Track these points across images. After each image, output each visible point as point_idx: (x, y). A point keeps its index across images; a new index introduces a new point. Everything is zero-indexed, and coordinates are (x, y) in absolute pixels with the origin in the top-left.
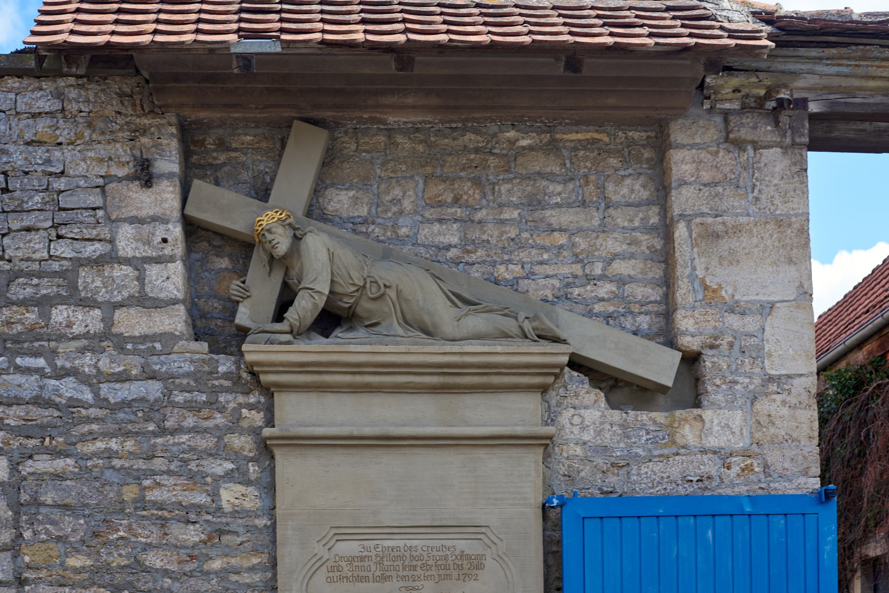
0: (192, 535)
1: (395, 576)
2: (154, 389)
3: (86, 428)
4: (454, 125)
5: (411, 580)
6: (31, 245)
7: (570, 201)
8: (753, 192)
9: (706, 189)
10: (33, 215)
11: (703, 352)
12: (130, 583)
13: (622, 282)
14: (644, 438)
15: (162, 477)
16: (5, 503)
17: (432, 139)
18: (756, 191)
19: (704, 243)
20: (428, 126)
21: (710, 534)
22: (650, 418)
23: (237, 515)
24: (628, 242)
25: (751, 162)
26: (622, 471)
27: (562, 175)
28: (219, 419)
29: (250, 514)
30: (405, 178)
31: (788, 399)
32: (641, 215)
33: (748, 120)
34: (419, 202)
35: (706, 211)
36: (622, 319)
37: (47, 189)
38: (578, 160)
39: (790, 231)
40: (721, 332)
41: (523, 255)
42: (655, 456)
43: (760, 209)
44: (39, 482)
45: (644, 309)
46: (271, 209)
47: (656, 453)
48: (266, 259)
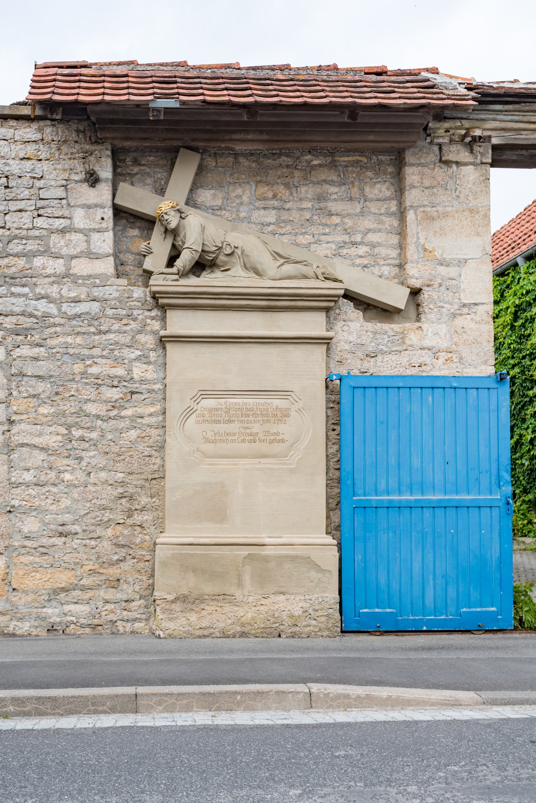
0: (114, 394)
1: (236, 420)
2: (95, 307)
3: (53, 330)
4: (274, 152)
5: (246, 422)
6: (22, 220)
7: (342, 197)
8: (455, 192)
9: (426, 191)
10: (24, 202)
11: (422, 288)
12: (77, 423)
13: (373, 246)
14: (386, 340)
15: (98, 359)
16: (2, 375)
17: (261, 160)
18: (457, 192)
19: (425, 223)
20: (259, 152)
21: (430, 399)
22: (390, 328)
23: (142, 382)
24: (378, 222)
25: (455, 174)
26: (372, 360)
27: (338, 182)
28: (133, 325)
29: (151, 382)
30: (244, 183)
31: (475, 318)
32: (385, 206)
33: (454, 148)
34: (252, 197)
35: (426, 203)
36: (373, 268)
37: (32, 187)
38: (348, 173)
39: (478, 216)
40: (434, 277)
41: (313, 229)
42: (393, 351)
43: (459, 203)
44: (24, 362)
45: (386, 262)
46: (168, 200)
47: (394, 349)
48: (163, 230)
